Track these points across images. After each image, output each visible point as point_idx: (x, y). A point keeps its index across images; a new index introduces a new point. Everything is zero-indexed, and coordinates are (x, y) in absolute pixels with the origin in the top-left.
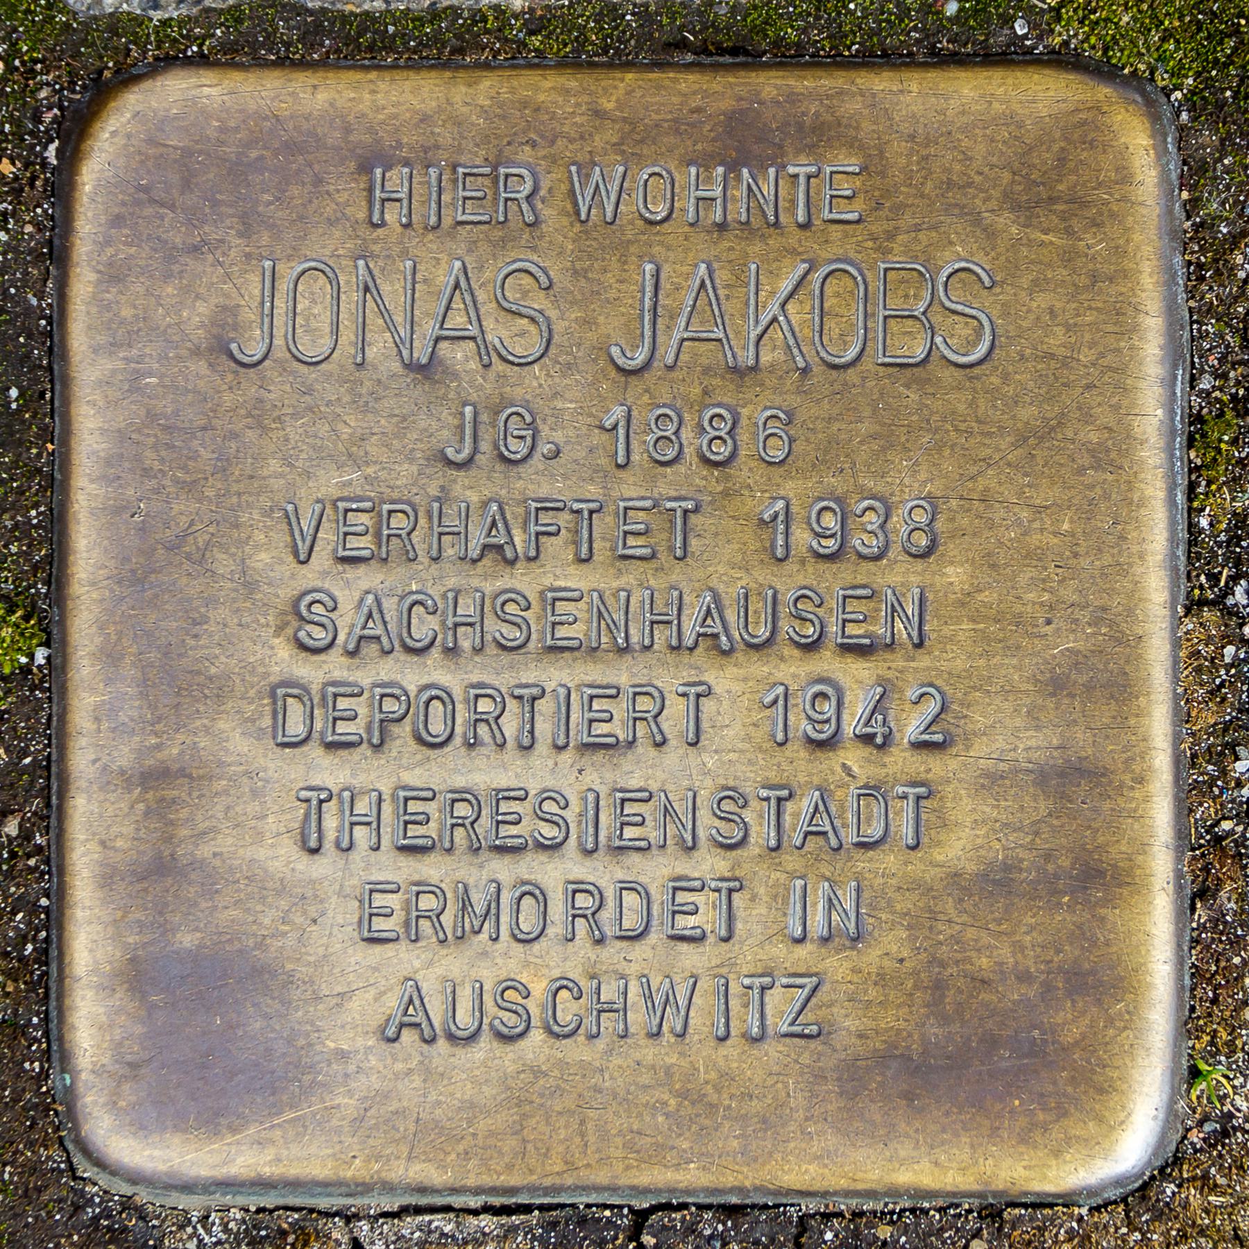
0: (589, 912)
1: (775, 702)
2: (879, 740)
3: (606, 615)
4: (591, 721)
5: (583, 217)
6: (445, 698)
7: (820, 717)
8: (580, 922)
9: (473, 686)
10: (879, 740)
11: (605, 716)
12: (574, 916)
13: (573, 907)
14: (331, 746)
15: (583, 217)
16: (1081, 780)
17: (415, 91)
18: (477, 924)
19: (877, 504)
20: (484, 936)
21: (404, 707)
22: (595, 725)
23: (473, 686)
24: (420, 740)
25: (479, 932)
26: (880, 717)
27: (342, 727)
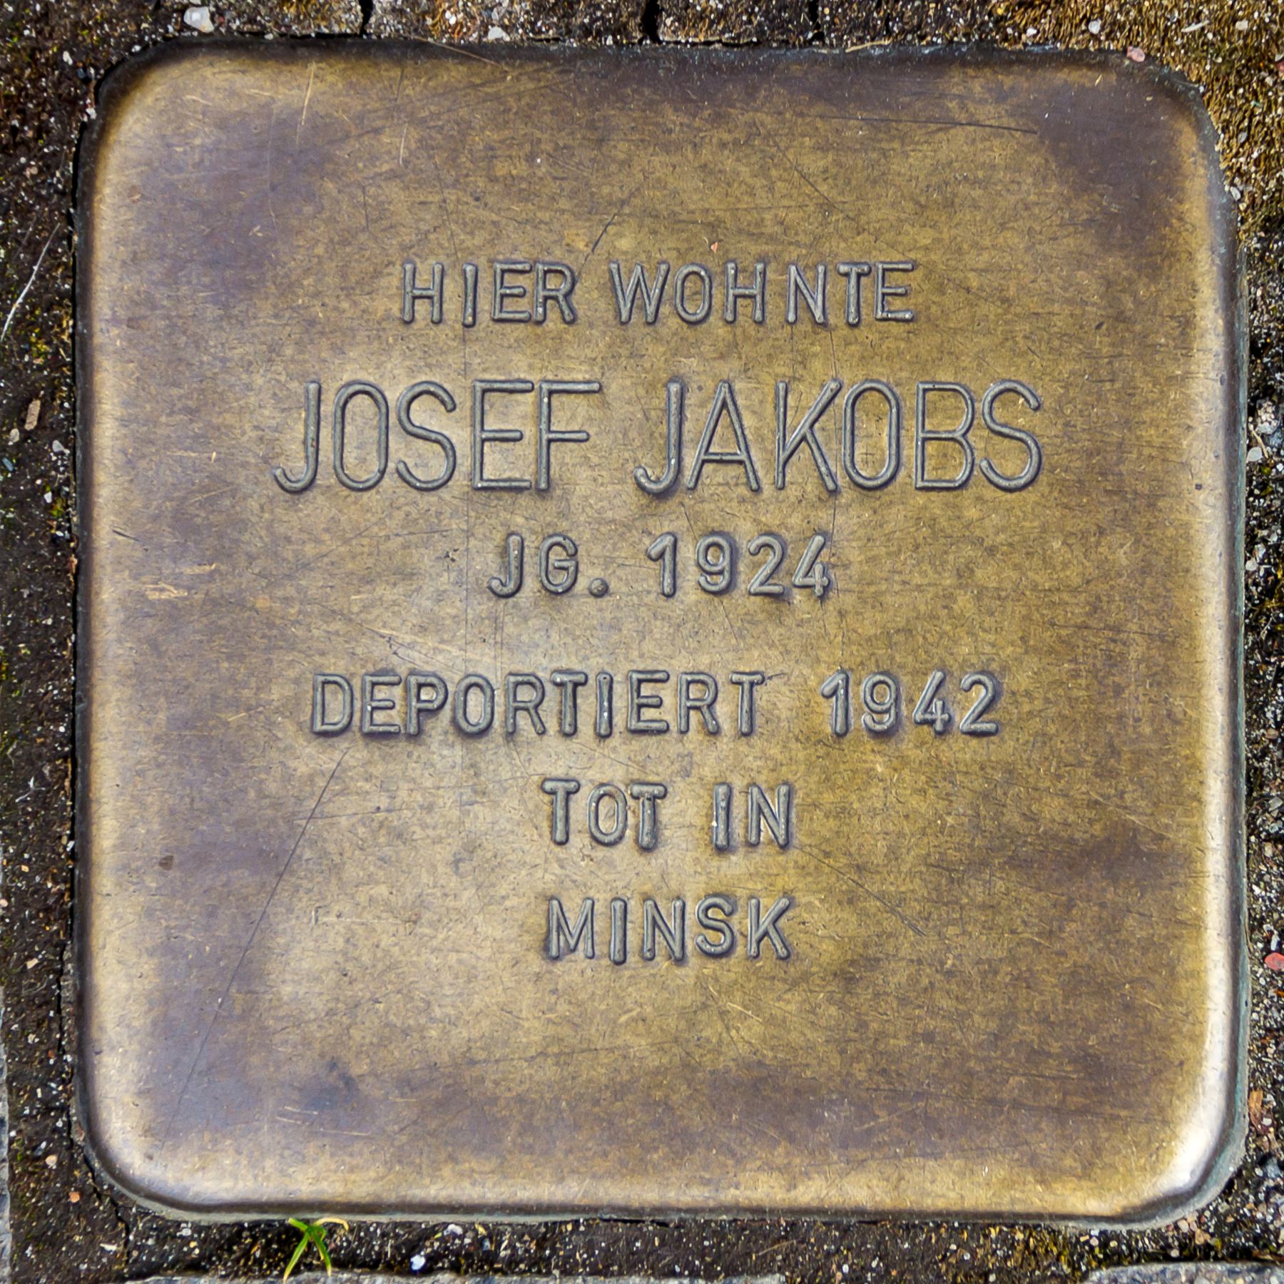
0: (530, 705)
1: (835, 692)
2: (939, 726)
3: (766, 810)
4: (640, 706)
5: (624, 318)
6: (482, 685)
7: (879, 708)
8: (521, 716)
9: (511, 674)
10: (939, 726)
11: (654, 701)
12: (516, 709)
13: (515, 700)
14: (372, 736)
15: (624, 318)
16: (1111, 648)
17: (1013, 1201)
18: (572, 942)
19: (984, 678)
20: (580, 953)
21: (441, 697)
22: (643, 710)
23: (511, 674)
24: (460, 731)
25: (574, 950)
26: (940, 704)
27: (380, 717)
